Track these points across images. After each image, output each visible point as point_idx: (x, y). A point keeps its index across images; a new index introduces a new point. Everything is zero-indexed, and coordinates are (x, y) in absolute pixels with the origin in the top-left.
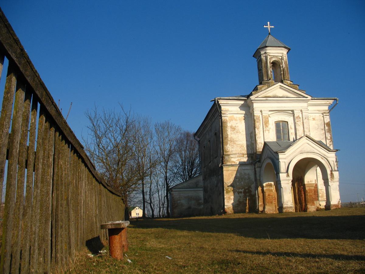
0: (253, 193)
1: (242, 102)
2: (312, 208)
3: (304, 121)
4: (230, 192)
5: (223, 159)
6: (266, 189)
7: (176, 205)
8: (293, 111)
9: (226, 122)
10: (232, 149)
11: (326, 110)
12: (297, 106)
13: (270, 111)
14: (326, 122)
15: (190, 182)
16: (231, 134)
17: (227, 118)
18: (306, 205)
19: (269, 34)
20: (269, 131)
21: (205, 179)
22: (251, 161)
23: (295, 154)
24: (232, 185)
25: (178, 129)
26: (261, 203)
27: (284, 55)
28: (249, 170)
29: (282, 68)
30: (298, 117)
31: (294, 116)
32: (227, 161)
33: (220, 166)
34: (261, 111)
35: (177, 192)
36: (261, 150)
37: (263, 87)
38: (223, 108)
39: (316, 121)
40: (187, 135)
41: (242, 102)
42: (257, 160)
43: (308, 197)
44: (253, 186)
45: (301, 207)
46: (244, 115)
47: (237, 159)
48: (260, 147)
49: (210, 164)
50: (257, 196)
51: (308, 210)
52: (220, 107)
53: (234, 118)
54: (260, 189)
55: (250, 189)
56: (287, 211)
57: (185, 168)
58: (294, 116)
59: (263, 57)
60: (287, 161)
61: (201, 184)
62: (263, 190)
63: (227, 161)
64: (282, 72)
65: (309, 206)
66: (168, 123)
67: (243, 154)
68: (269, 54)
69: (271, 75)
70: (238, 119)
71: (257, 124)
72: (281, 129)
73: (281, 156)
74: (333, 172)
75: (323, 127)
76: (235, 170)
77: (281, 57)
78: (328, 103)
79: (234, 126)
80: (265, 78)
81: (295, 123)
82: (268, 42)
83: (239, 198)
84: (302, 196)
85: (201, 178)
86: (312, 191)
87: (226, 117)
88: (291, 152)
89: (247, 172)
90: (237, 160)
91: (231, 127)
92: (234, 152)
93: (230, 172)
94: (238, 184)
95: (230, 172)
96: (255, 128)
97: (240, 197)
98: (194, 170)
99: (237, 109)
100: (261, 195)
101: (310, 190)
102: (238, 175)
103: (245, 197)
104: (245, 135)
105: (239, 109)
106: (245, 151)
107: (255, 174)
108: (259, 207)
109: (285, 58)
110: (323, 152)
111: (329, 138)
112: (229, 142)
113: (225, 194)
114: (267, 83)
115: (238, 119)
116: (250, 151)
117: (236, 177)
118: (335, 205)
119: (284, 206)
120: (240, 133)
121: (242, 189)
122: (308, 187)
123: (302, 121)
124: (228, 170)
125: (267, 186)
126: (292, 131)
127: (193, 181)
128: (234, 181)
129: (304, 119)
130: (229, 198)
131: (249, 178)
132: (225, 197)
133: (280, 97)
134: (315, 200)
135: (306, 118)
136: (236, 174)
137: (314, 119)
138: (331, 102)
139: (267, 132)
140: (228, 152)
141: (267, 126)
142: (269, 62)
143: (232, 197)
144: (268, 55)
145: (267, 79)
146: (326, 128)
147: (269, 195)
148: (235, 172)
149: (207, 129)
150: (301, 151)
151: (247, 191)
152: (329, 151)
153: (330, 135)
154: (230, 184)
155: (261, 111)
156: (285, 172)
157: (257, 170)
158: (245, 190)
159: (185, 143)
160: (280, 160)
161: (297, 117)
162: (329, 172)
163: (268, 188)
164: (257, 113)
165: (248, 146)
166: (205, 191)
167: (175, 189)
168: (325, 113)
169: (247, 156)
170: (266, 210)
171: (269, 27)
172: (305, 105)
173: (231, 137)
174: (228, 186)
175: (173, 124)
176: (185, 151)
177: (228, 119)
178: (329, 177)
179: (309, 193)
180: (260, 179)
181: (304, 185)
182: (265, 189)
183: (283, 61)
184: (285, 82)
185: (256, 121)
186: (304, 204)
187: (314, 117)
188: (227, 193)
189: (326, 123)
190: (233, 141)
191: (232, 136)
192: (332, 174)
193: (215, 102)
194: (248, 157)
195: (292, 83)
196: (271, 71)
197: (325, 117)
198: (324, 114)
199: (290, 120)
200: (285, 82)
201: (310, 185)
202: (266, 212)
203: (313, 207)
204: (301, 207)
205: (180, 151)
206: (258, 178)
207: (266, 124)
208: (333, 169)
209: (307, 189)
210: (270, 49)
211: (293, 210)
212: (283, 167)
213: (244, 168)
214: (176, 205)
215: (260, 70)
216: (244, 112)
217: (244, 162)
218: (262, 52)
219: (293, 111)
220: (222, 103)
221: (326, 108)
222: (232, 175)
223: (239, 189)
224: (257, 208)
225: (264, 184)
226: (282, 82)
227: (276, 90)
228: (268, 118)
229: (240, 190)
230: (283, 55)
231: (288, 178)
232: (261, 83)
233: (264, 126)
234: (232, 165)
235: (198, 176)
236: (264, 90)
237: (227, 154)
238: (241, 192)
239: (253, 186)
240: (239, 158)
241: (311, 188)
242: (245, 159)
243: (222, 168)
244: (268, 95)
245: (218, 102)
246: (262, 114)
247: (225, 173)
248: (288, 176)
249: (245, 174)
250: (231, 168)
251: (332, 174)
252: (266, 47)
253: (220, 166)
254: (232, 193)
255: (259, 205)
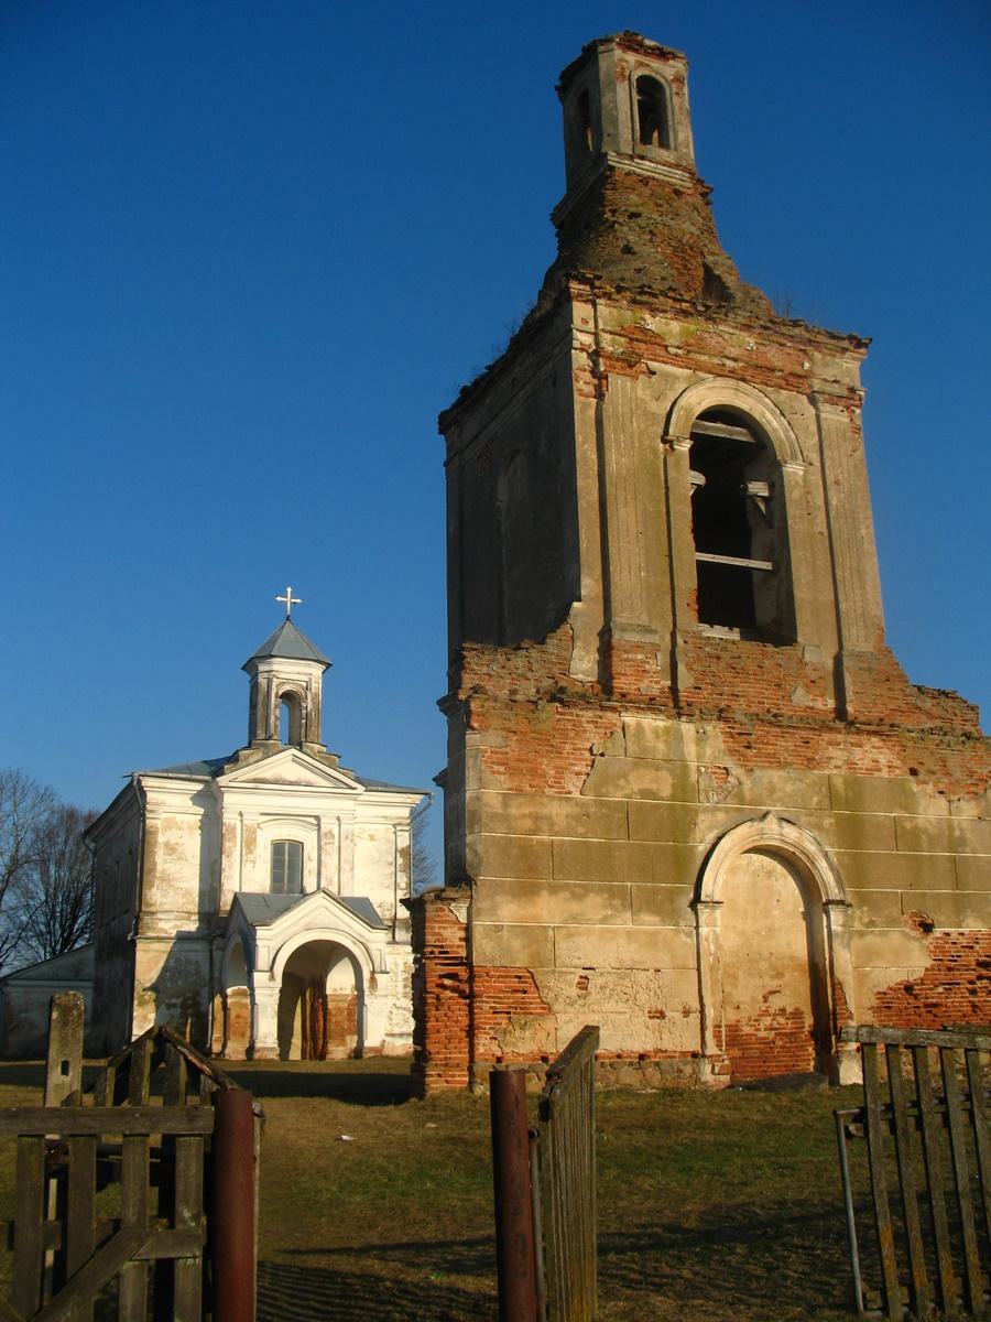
0: (202, 1009)
1: (200, 787)
2: (338, 1052)
3: (342, 844)
4: (147, 1003)
5: (137, 923)
6: (233, 1003)
7: (14, 1024)
8: (317, 818)
9: (156, 833)
10: (164, 900)
11: (403, 818)
12: (329, 806)
13: (262, 814)
14: (400, 846)
15: (61, 962)
16: (165, 861)
17: (159, 824)
18: (325, 1044)
19: (288, 619)
20: (254, 862)
21: (99, 958)
22: (206, 932)
23: (295, 929)
24: (154, 988)
25: (45, 796)
26: (217, 1034)
27: (313, 679)
28: (199, 953)
29: (304, 711)
30: (330, 834)
31: (319, 830)
32: (148, 928)
33: (129, 938)
34: (241, 814)
35: (21, 989)
36: (228, 908)
37: (252, 754)
38: (150, 796)
39: (376, 843)
40: (71, 816)
41: (200, 787)
42: (219, 932)
43: (331, 1026)
44: (205, 992)
45: (315, 1049)
46: (200, 817)
47: (172, 924)
48: (226, 901)
49: (113, 924)
50: (210, 1018)
51: (328, 1056)
52: (144, 794)
53: (177, 823)
54: (218, 1000)
55: (198, 999)
56: (264, 1057)
57: (53, 912)
58: (319, 830)
59: (262, 680)
60: (274, 945)
61: (90, 970)
62: (224, 1004)
63: (148, 928)
64: (304, 721)
65: (331, 1047)
66: (18, 776)
67: (188, 913)
68: (277, 674)
69: (276, 726)
70: (185, 826)
71: (227, 845)
72: (287, 858)
73: (261, 932)
74: (376, 975)
75: (392, 859)
76: (164, 952)
77: (304, 684)
78: (409, 801)
79: (173, 842)
80: (261, 734)
81: (320, 848)
82: (278, 643)
83: (168, 1018)
84: (318, 1021)
85: (91, 954)
86: (342, 1012)
87: (155, 820)
88: (288, 924)
89: (194, 957)
90: (173, 928)
91: (167, 844)
92: (167, 907)
93: (151, 955)
94: (169, 984)
95: (151, 955)
96: (221, 853)
97: (172, 1017)
98: (79, 921)
99: (185, 802)
100: (219, 1015)
101: (339, 1009)
102: (172, 964)
103: (184, 1016)
104: (198, 867)
105: (191, 803)
106: (193, 904)
107: (211, 964)
108: (214, 1043)
109: (317, 686)
110: (359, 928)
111: (403, 885)
112: (157, 882)
113: (135, 1007)
114: (262, 745)
115: (185, 826)
116: (207, 905)
117: (165, 969)
118: (372, 1049)
119: (258, 1045)
120: (186, 860)
121: (177, 997)
122: (333, 1001)
123: (337, 844)
124: (148, 951)
125: (235, 994)
126: (310, 866)
127: (67, 961)
128: (161, 977)
129: (343, 839)
130: (145, 1018)
131: (198, 972)
132: (135, 1014)
133: (291, 784)
134: (349, 1034)
135: (347, 838)
136: (167, 961)
137: (372, 838)
138: (417, 799)
139: (249, 865)
140: (151, 905)
141: (251, 852)
142: (273, 695)
143: (152, 1016)
144: (274, 676)
145: (264, 736)
146: (400, 861)
147: (238, 1017)
148: (165, 956)
149: (116, 829)
150: (309, 923)
151: (190, 1002)
152: (373, 928)
153: (405, 879)
154: (148, 985)
155: (241, 814)
156: (267, 968)
157: (218, 955)
158: (186, 1000)
159: (61, 839)
160: (258, 942)
161: (326, 834)
162: (366, 975)
163: (237, 999)
164: (229, 818)
165: (202, 894)
166: (98, 990)
167: (15, 979)
168: (399, 824)
169: (196, 917)
170: (226, 1051)
171: (288, 599)
172: (348, 804)
173: (164, 870)
174: (144, 990)
175: (30, 781)
176: (59, 865)
177: (159, 826)
178: (366, 985)
179: (334, 1015)
180: (220, 978)
181: (325, 997)
182: (229, 1001)
183: (309, 694)
184: (307, 747)
185: (227, 836)
186: (321, 1042)
187: (371, 833)
188: (140, 1005)
189: (399, 849)
190: (166, 879)
191: (167, 866)
192: (373, 979)
193: (132, 781)
194: (200, 920)
195: (324, 749)
196: (276, 716)
197: (398, 833)
198: (399, 828)
199: (308, 839)
200: (307, 747)
201: (337, 998)
202: (227, 1057)
203: (341, 1048)
204: (315, 1049)
205: (44, 862)
206: (217, 975)
207: (248, 848)
208: (377, 969)
209: (331, 1005)
210: (281, 663)
211: (274, 1056)
212: (263, 957)
213: (187, 946)
214: (14, 1024)
215: (253, 706)
216: (202, 811)
217: (190, 932)
218: (262, 668)
219: (317, 818)
220: (150, 784)
221: (406, 812)
222: (157, 963)
223: (172, 997)
224: (208, 1046)
225: (229, 991)
226: (300, 746)
227: (284, 764)
228: (255, 832)
229: (174, 1001)
230: (310, 679)
231: (271, 984)
232: (249, 746)
233: (244, 850)
234: (160, 939)
235: (83, 947)
236: (255, 762)
237: (148, 910)
238: (174, 1005)
239: (205, 992)
240: (179, 923)
241: (340, 1004)
242: (192, 926)
243: (133, 944)
244: (261, 776)
245: (139, 782)
246: (241, 821)
247: (140, 956)
248: (272, 978)
249: (189, 961)
250: (156, 946)
251: (373, 979)
252: (273, 656)
253: (129, 938)
254: (152, 1006)
255: (214, 1038)
